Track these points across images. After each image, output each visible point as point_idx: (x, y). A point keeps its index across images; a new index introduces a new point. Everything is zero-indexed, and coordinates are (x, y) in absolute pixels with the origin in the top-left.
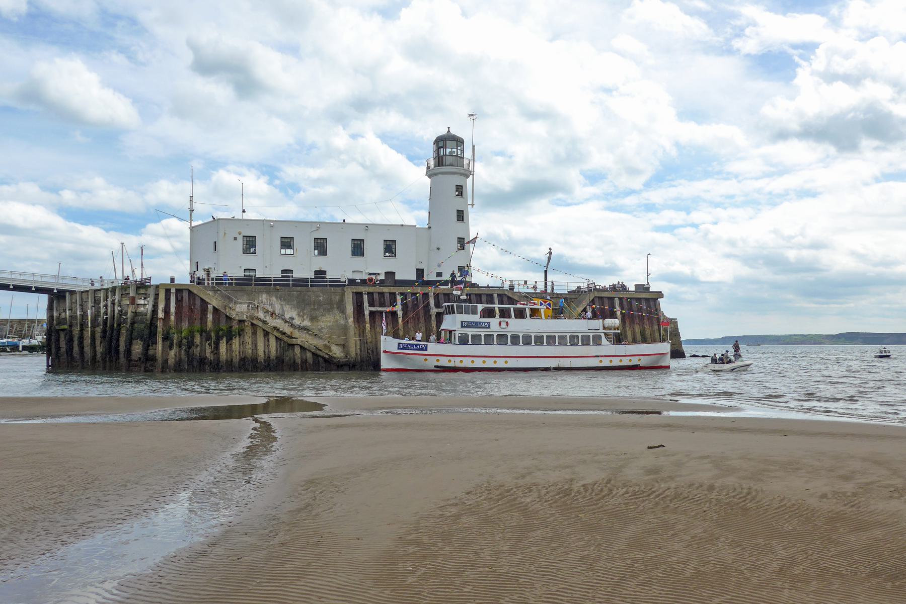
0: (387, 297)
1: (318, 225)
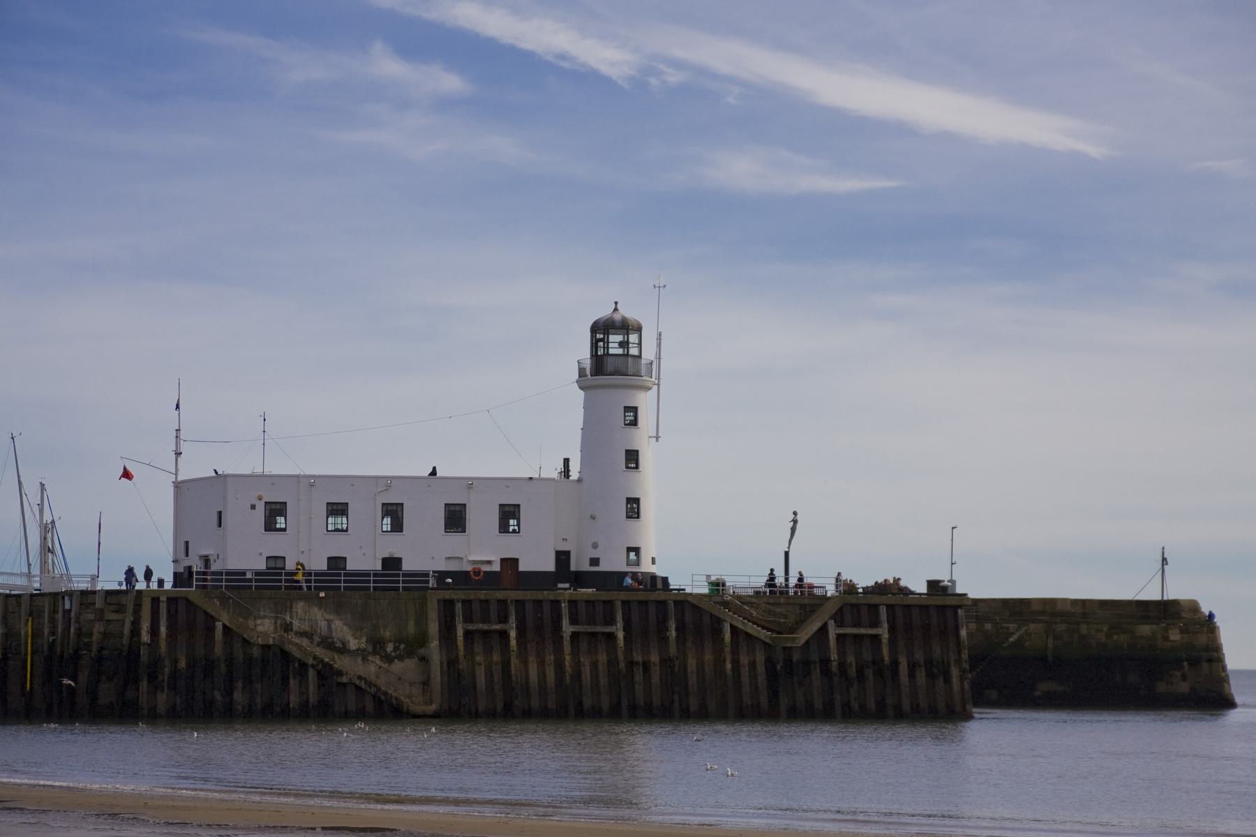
0: (493, 608)
1: (388, 482)
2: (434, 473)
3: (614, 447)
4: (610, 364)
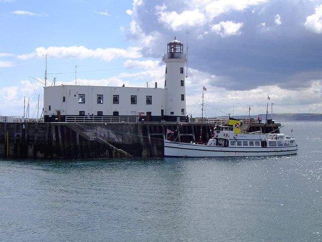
2: (124, 86)
3: (176, 79)
4: (176, 55)
